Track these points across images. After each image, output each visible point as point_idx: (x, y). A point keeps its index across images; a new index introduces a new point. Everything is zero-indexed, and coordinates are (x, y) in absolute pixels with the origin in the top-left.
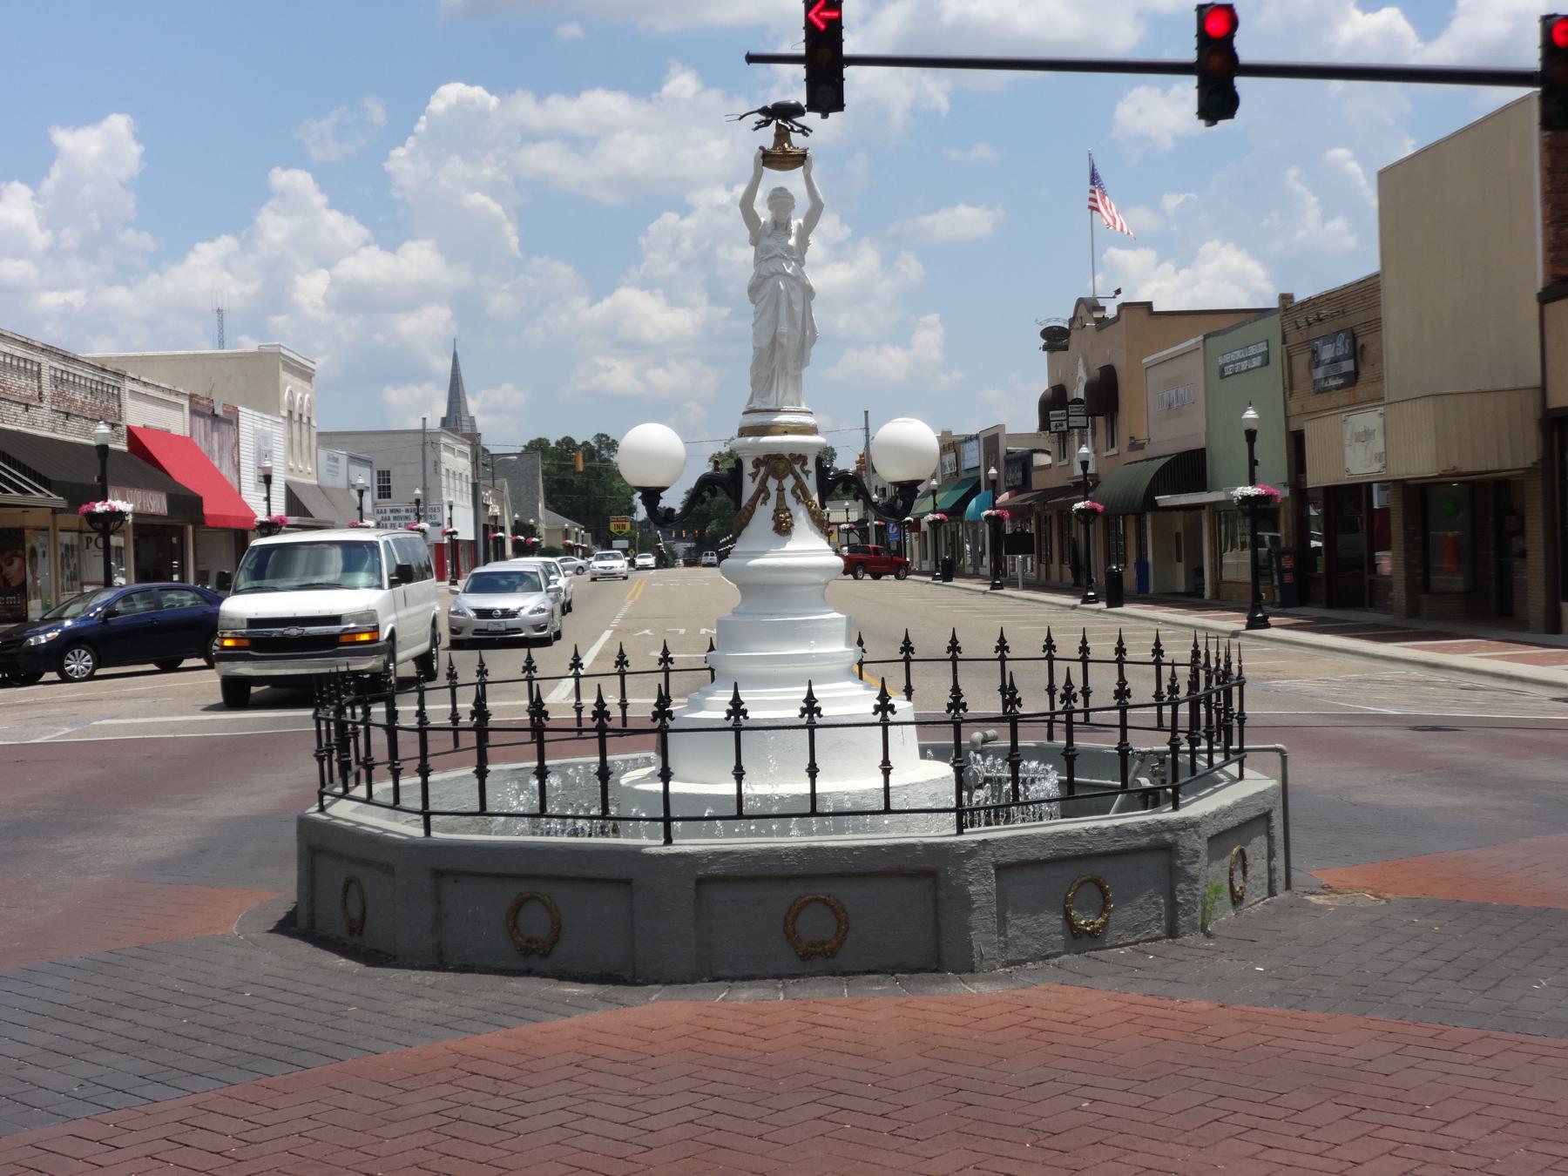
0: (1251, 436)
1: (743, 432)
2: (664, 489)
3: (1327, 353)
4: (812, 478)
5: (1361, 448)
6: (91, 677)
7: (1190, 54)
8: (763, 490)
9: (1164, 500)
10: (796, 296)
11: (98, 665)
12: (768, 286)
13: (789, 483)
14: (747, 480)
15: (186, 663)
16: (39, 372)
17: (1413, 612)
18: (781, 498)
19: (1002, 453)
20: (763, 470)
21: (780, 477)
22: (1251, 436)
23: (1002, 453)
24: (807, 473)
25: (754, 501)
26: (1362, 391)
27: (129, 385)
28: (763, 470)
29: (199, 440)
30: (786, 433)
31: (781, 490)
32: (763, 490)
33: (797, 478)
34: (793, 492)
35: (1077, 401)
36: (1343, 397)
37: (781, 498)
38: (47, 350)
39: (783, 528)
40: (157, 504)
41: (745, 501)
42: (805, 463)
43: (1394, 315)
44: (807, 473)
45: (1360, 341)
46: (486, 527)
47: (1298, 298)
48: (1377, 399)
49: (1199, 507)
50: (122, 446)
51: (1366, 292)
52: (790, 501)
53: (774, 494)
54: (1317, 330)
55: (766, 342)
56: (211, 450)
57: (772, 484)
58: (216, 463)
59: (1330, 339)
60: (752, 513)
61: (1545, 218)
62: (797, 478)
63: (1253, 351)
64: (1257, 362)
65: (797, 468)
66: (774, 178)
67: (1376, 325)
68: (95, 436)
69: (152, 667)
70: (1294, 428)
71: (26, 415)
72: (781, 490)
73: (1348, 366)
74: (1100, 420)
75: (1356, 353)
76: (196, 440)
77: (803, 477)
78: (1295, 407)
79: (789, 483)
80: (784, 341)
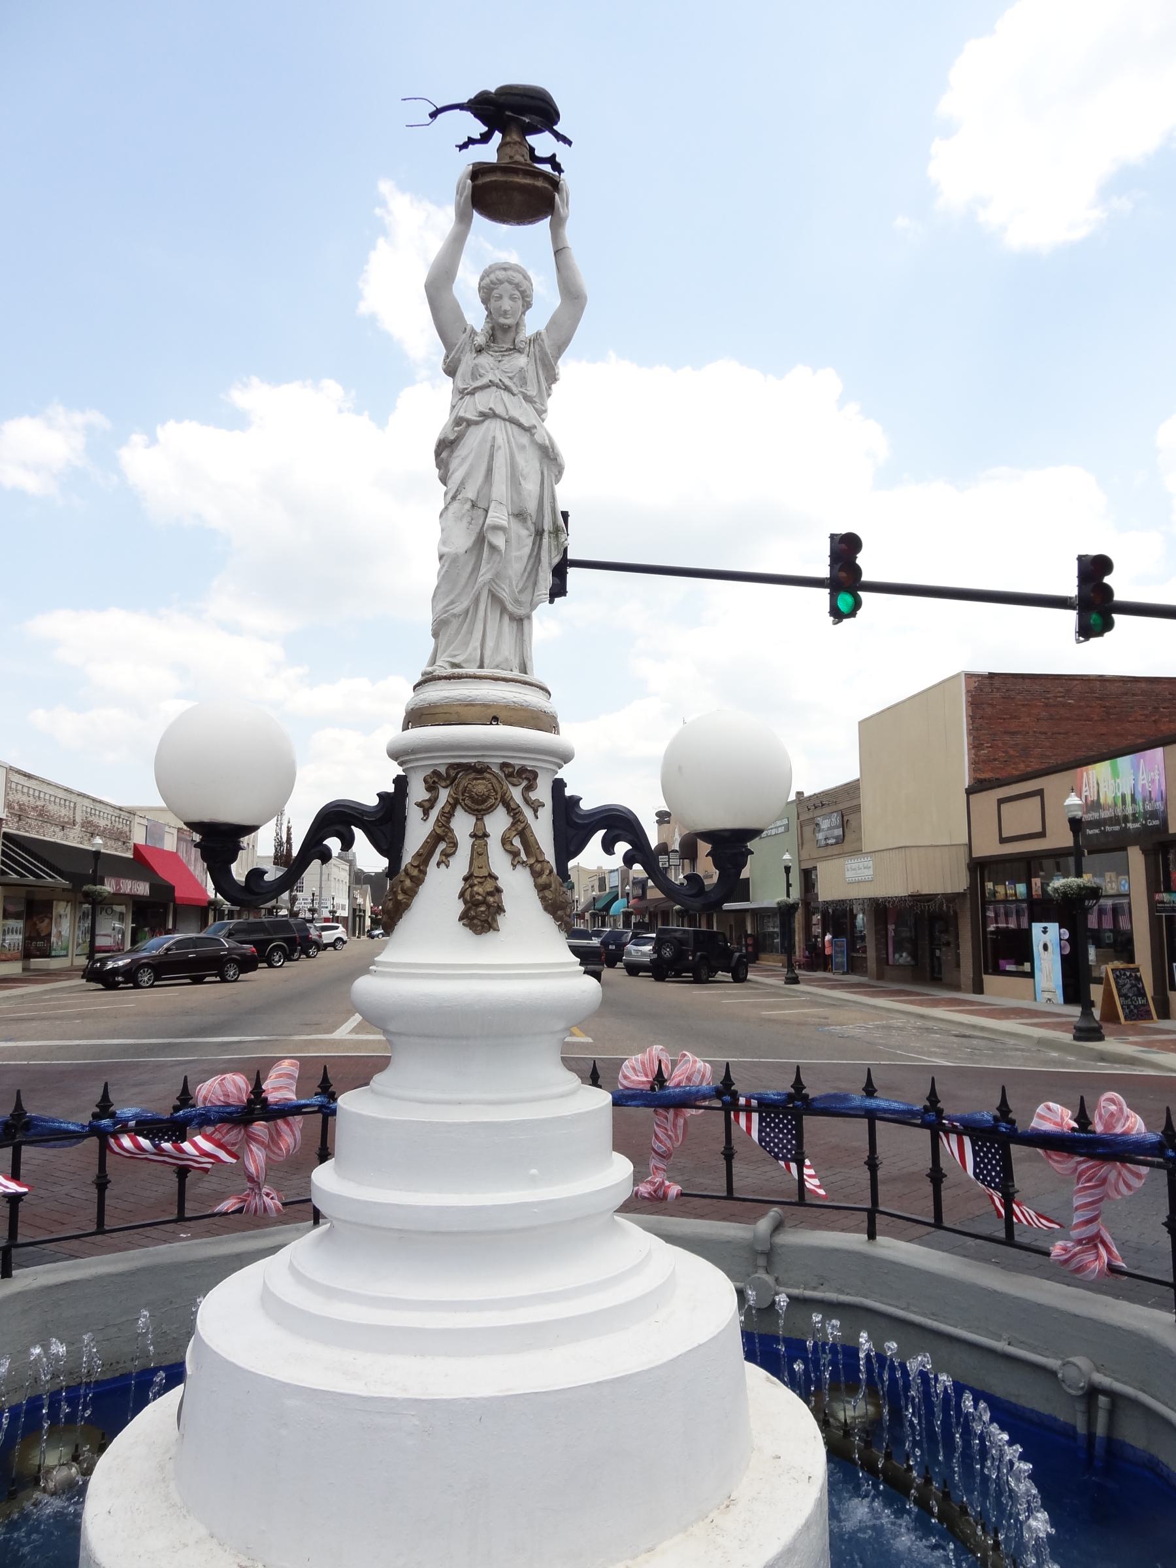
0: (788, 869)
1: (416, 717)
2: (252, 829)
3: (825, 824)
4: (546, 814)
5: (849, 879)
6: (152, 986)
7: (824, 572)
8: (442, 837)
9: (727, 906)
10: (529, 464)
11: (157, 978)
12: (474, 439)
13: (498, 823)
14: (413, 814)
15: (207, 979)
16: (75, 808)
17: (880, 976)
18: (479, 853)
19: (631, 879)
20: (444, 795)
21: (479, 808)
22: (788, 869)
23: (631, 879)
24: (535, 807)
25: (424, 857)
26: (847, 846)
27: (137, 820)
28: (444, 795)
29: (182, 855)
30: (495, 720)
31: (480, 836)
32: (442, 837)
33: (514, 812)
34: (505, 841)
35: (673, 851)
36: (836, 850)
37: (479, 853)
38: (80, 795)
39: (481, 911)
40: (142, 889)
41: (407, 858)
42: (530, 787)
43: (868, 802)
44: (535, 807)
45: (846, 818)
46: (354, 910)
47: (806, 795)
48: (857, 852)
49: (746, 911)
50: (130, 855)
51: (851, 790)
52: (498, 861)
53: (465, 845)
54: (818, 812)
55: (463, 541)
56: (190, 860)
57: (462, 824)
58: (192, 868)
59: (834, 815)
60: (418, 881)
61: (969, 744)
62: (514, 812)
63: (779, 823)
64: (781, 830)
65: (516, 793)
66: (499, 243)
67: (857, 809)
68: (93, 845)
69: (188, 981)
70: (805, 866)
71: (61, 833)
72: (480, 836)
73: (839, 832)
74: (687, 861)
75: (844, 824)
76: (180, 854)
77: (528, 813)
78: (805, 855)
79: (498, 823)
80: (499, 540)
